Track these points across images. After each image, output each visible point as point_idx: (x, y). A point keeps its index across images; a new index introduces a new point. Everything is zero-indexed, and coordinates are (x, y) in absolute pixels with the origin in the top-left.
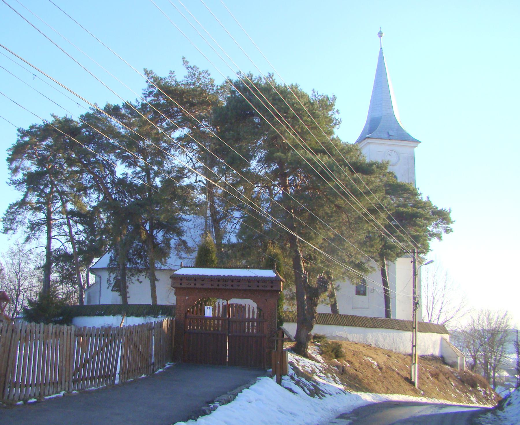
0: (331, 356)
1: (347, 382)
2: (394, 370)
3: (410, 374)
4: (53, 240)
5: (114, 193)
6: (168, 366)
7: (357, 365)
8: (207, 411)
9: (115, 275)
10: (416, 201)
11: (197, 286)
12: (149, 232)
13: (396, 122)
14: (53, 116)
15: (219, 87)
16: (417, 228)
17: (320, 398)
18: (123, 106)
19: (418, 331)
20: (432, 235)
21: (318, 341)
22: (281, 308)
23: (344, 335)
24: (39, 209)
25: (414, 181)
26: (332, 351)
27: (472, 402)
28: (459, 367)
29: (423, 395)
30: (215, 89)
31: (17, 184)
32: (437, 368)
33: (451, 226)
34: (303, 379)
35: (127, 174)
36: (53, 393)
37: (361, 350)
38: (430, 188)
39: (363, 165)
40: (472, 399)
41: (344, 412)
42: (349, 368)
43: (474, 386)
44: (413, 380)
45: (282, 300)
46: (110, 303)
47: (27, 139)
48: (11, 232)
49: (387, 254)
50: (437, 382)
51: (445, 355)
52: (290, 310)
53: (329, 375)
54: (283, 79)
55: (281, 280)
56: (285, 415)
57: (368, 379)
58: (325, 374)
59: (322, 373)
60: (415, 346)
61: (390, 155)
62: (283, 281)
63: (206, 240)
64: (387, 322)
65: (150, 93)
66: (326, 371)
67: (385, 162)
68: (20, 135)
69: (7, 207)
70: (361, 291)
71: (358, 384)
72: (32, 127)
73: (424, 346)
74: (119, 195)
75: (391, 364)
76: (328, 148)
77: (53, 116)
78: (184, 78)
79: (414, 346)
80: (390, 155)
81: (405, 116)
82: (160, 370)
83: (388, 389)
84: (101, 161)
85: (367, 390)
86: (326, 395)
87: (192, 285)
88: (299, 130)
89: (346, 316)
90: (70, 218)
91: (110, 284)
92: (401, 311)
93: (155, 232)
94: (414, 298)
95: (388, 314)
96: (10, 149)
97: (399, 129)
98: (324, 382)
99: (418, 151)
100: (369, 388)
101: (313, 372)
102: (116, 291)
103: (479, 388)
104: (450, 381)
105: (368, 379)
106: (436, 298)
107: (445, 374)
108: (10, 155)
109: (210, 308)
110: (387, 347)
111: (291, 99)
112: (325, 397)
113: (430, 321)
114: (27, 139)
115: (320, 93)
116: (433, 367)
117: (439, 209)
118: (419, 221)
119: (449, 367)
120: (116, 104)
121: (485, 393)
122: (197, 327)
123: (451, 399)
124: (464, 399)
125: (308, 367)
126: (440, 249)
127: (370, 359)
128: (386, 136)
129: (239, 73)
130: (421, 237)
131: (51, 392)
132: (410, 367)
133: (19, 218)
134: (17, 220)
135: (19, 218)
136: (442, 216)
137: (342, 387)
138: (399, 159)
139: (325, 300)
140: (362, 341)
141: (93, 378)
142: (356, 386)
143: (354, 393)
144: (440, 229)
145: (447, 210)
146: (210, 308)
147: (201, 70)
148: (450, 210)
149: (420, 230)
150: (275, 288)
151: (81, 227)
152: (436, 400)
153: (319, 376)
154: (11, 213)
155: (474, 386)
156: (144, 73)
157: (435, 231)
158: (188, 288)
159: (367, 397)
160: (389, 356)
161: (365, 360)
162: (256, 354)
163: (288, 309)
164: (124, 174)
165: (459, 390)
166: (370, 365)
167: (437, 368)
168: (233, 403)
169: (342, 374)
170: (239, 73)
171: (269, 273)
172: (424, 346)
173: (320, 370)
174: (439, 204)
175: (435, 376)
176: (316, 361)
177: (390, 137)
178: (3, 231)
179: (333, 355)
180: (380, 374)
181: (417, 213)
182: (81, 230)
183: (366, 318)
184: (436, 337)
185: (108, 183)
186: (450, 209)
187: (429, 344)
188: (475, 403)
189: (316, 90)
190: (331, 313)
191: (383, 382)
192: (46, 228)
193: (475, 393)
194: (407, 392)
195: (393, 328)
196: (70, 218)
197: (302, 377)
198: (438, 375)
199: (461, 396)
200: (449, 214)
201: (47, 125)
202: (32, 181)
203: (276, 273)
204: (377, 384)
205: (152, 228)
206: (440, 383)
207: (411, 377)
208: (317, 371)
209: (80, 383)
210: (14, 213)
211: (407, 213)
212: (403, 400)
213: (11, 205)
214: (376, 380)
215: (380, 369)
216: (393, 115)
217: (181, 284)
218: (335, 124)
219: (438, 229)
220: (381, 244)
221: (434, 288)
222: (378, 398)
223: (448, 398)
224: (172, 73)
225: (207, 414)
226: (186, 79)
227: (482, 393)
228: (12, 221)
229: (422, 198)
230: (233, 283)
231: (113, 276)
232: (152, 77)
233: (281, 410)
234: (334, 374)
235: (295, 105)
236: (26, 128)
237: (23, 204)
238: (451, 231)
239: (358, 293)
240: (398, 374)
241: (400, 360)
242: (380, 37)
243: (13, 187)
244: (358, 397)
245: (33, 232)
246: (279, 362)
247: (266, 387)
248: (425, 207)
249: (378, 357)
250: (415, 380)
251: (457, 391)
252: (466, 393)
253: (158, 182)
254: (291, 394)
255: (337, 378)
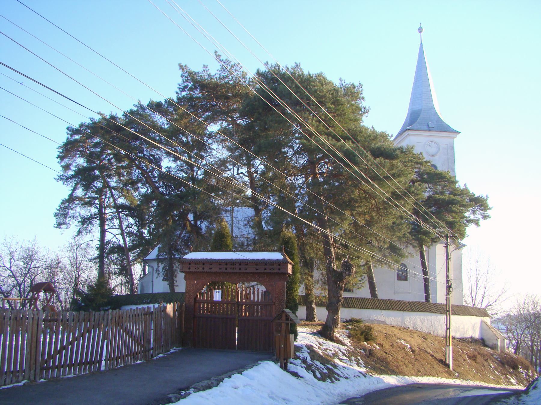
0: (359, 339)
1: (371, 365)
2: (427, 353)
3: (445, 356)
4: (107, 234)
5: (161, 187)
6: (172, 351)
7: (388, 347)
8: (173, 399)
9: (163, 265)
10: (453, 189)
11: (206, 270)
12: (192, 222)
13: (436, 114)
14: (100, 114)
15: (251, 80)
16: (454, 215)
17: (333, 382)
18: (166, 102)
19: (452, 314)
20: (469, 221)
21: (350, 325)
22: (295, 291)
23: (382, 319)
24: (90, 204)
25: (454, 170)
26: (362, 334)
27: (511, 384)
28: (499, 349)
29: (458, 377)
30: (247, 81)
31: (65, 179)
32: (475, 350)
33: (488, 212)
34: (318, 363)
35: (170, 168)
36: (11, 383)
37: (395, 333)
38: (467, 177)
39: (387, 150)
40: (512, 380)
41: (354, 396)
42: (378, 351)
43: (515, 367)
44: (447, 362)
45: (296, 283)
46: (162, 292)
47: (77, 137)
48: (63, 226)
49: (420, 238)
50: (474, 364)
51: (485, 338)
52: (323, 295)
53: (353, 358)
54: (310, 68)
55: (289, 263)
56: (277, 401)
57: (398, 362)
58: (349, 357)
59: (346, 356)
60: (449, 329)
61: (430, 146)
62: (290, 264)
63: (221, 226)
64: (426, 306)
65: (186, 87)
66: (350, 354)
67: (409, 147)
68: (70, 133)
69: (59, 203)
70: (402, 277)
71: (385, 367)
72: (81, 125)
73: (463, 328)
74: (166, 188)
75: (425, 346)
76: (356, 135)
77: (100, 114)
78: (217, 72)
79: (448, 329)
80: (430, 146)
81: (444, 108)
82: (161, 355)
83: (419, 371)
84: (149, 156)
85: (392, 372)
86: (341, 379)
87: (201, 270)
88: (323, 117)
89: (384, 301)
90: (121, 212)
91: (159, 274)
92: (440, 298)
93: (199, 223)
94: (448, 282)
95: (427, 298)
96: (60, 147)
97: (439, 120)
98: (345, 365)
99: (458, 142)
100: (397, 371)
101: (335, 355)
102: (165, 280)
103: (521, 370)
104: (488, 363)
105: (398, 362)
106: (480, 283)
107: (483, 356)
108: (60, 153)
109: (219, 292)
110: (425, 330)
111: (314, 86)
112: (339, 380)
113: (474, 305)
114: (77, 137)
115: (347, 82)
116: (471, 349)
117: (476, 196)
118: (455, 208)
119: (489, 349)
120: (158, 101)
121: (527, 375)
122: (207, 310)
123: (489, 381)
124: (503, 380)
125: (331, 350)
126: (476, 237)
127: (403, 342)
128: (426, 128)
129: (267, 64)
130: (456, 223)
131: (8, 381)
132: (445, 349)
133: (71, 212)
134: (70, 215)
135: (71, 212)
136: (480, 203)
137: (363, 370)
138: (439, 150)
139: (356, 284)
140: (400, 324)
141: (71, 365)
142: (381, 369)
143: (377, 376)
144: (478, 216)
145: (484, 196)
146: (219, 292)
147: (232, 63)
148: (487, 197)
149: (457, 216)
150: (282, 271)
151: (131, 220)
152: (471, 382)
153: (341, 360)
154: (64, 208)
155: (515, 367)
156: (179, 68)
157: (472, 217)
158: (197, 272)
159: (391, 380)
160: (425, 338)
161: (398, 343)
162: (264, 337)
163: (321, 293)
164: (167, 167)
165: (499, 372)
166: (403, 348)
167: (475, 350)
168: (214, 390)
169: (368, 357)
170: (267, 64)
171: (277, 256)
172: (463, 328)
173: (343, 353)
174: (476, 191)
175: (473, 358)
176: (343, 344)
177: (429, 129)
178: (56, 226)
179: (362, 338)
180: (413, 356)
181: (453, 200)
182: (132, 223)
183: (404, 303)
184: (476, 320)
185: (155, 177)
186: (487, 196)
187: (466, 327)
188: (515, 385)
189: (343, 79)
190: (370, 297)
191: (413, 365)
192: (98, 222)
193: (516, 375)
194: (439, 375)
195: (431, 312)
196: (121, 212)
197: (317, 360)
198: (476, 357)
199: (500, 378)
200: (486, 200)
201: (95, 123)
202: (84, 177)
203: (284, 255)
204: (407, 366)
205: (196, 219)
206: (477, 365)
207: (446, 359)
208: (341, 354)
209: (54, 371)
210: (67, 208)
211: (443, 200)
212: (433, 383)
213: (63, 200)
214: (407, 362)
215: (413, 351)
216: (433, 108)
217: (189, 268)
218: (364, 113)
219: (476, 216)
220: (409, 228)
221: (478, 273)
222: (403, 381)
223: (485, 380)
224: (205, 67)
225: (172, 402)
226: (219, 73)
227: (524, 375)
228: (65, 216)
229: (459, 186)
230: (240, 267)
231: (161, 266)
232: (187, 72)
233: (273, 396)
234: (359, 358)
235: (318, 92)
236: (76, 126)
237: (71, 199)
238: (489, 217)
239: (400, 278)
240: (432, 356)
241: (436, 343)
242: (421, 32)
243: (61, 182)
244: (379, 381)
245: (85, 226)
246: (282, 346)
247: (268, 371)
248: (462, 194)
249: (413, 339)
250: (449, 362)
251: (497, 372)
252: (506, 375)
253: (200, 175)
254: (294, 379)
255: (361, 361)
